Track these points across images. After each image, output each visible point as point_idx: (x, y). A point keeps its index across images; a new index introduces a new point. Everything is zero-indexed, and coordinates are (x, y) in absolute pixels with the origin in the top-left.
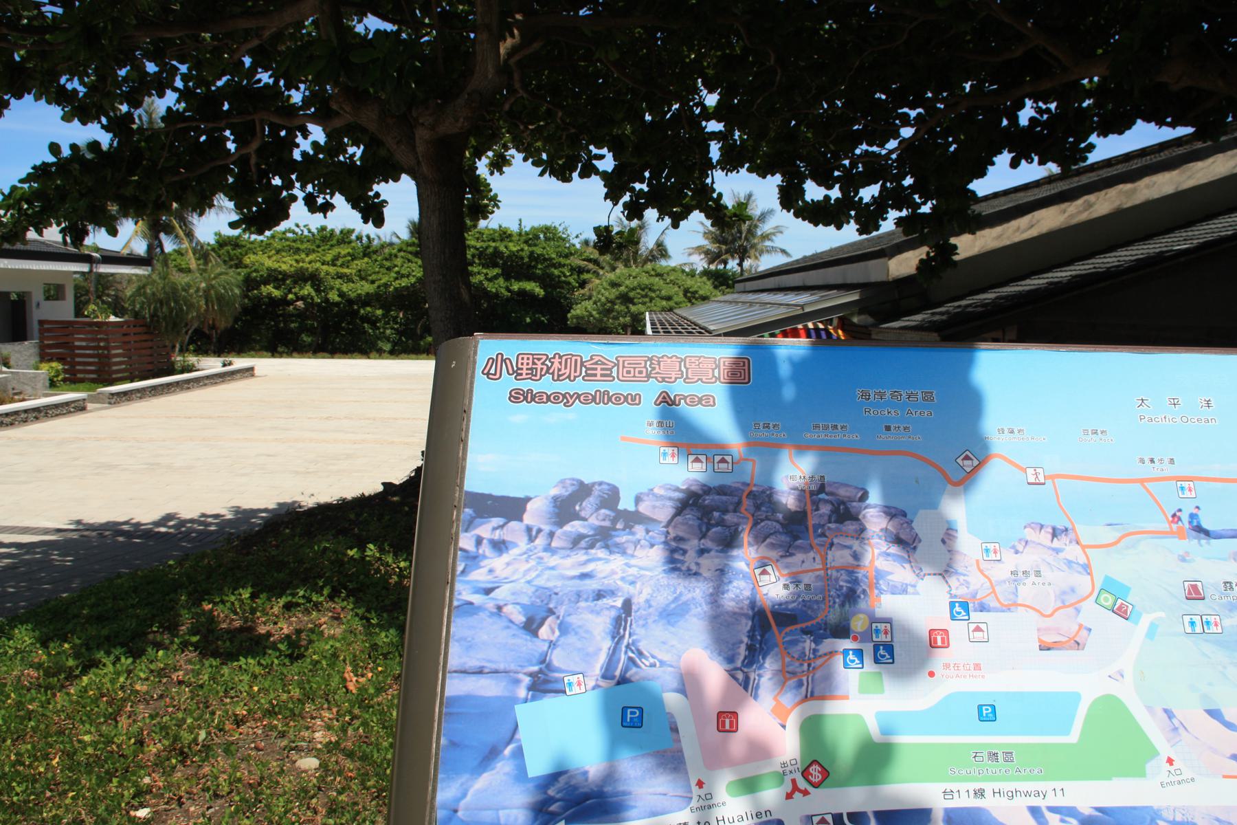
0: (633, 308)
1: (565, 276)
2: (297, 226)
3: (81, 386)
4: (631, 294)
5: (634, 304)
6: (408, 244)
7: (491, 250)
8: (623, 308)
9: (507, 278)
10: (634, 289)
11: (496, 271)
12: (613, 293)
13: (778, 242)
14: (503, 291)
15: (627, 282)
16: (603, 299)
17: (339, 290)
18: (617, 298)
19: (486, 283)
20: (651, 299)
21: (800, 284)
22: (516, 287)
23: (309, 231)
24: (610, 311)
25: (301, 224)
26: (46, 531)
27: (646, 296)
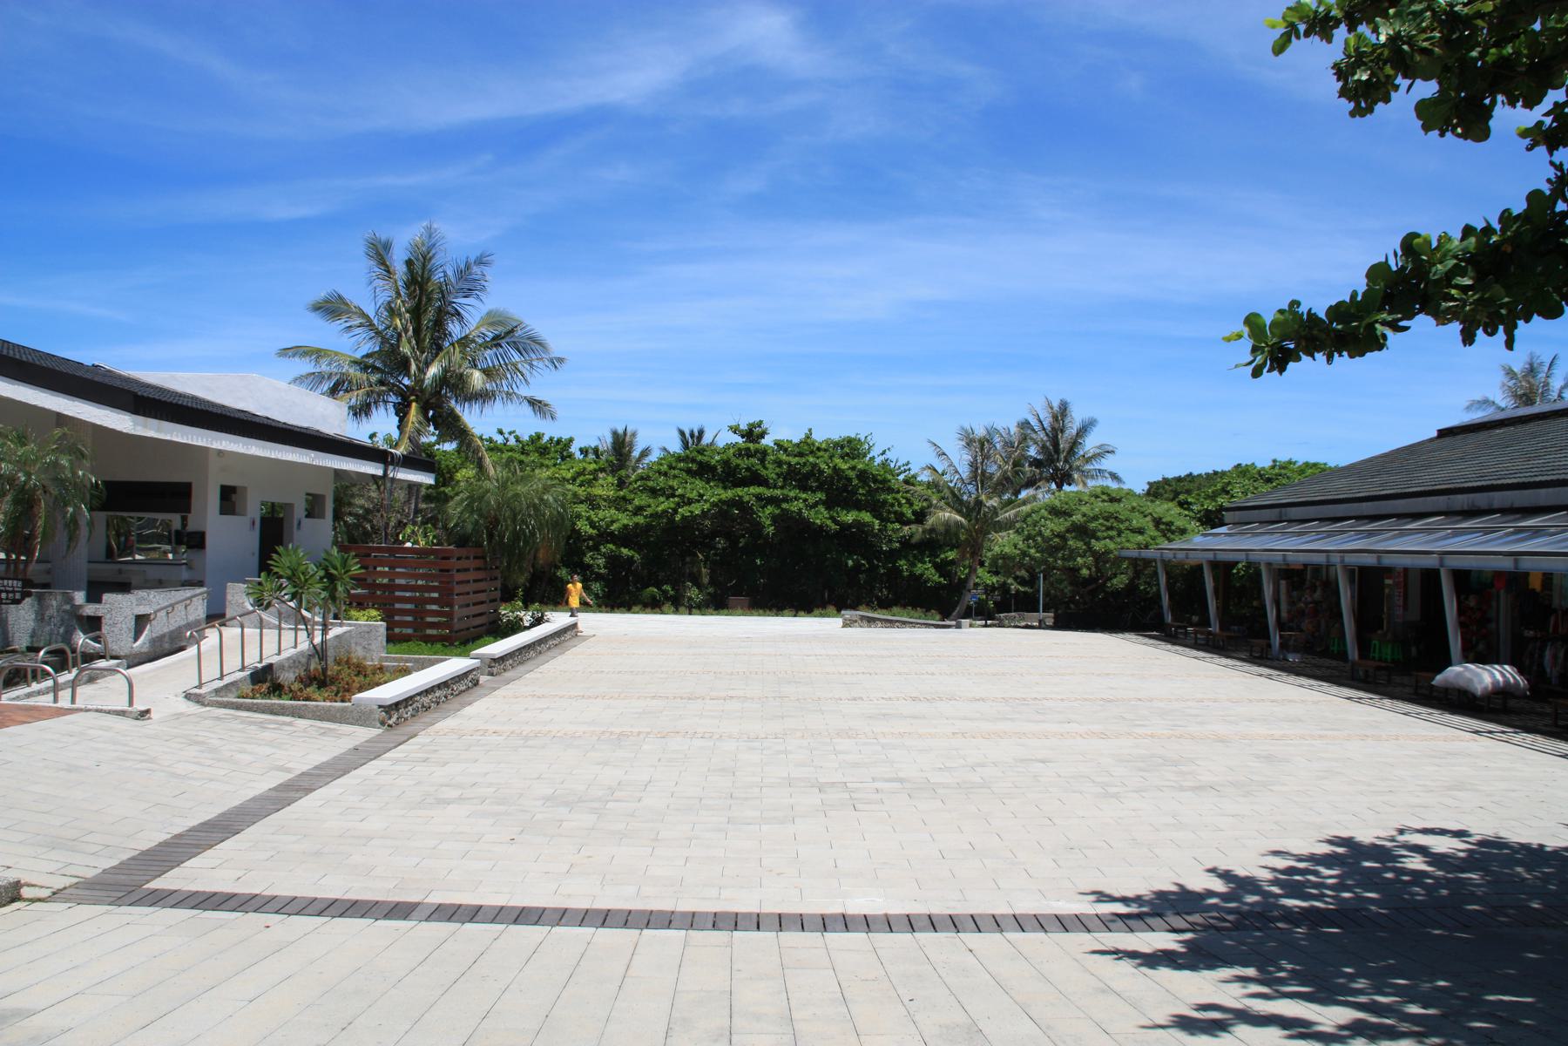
0: (1098, 546)
1: (900, 505)
2: (501, 432)
3: (405, 646)
4: (1093, 525)
5: (1098, 539)
6: (679, 459)
7: (808, 468)
8: (1080, 544)
9: (829, 504)
10: (1095, 518)
11: (820, 496)
12: (1059, 525)
13: (1107, 464)
14: (829, 522)
15: (1084, 509)
16: (1047, 533)
17: (588, 518)
18: (1068, 531)
19: (805, 513)
20: (1120, 533)
21: (1507, 505)
22: (849, 517)
23: (518, 440)
24: (1057, 549)
25: (506, 431)
26: (1125, 900)
27: (1111, 528)
